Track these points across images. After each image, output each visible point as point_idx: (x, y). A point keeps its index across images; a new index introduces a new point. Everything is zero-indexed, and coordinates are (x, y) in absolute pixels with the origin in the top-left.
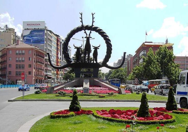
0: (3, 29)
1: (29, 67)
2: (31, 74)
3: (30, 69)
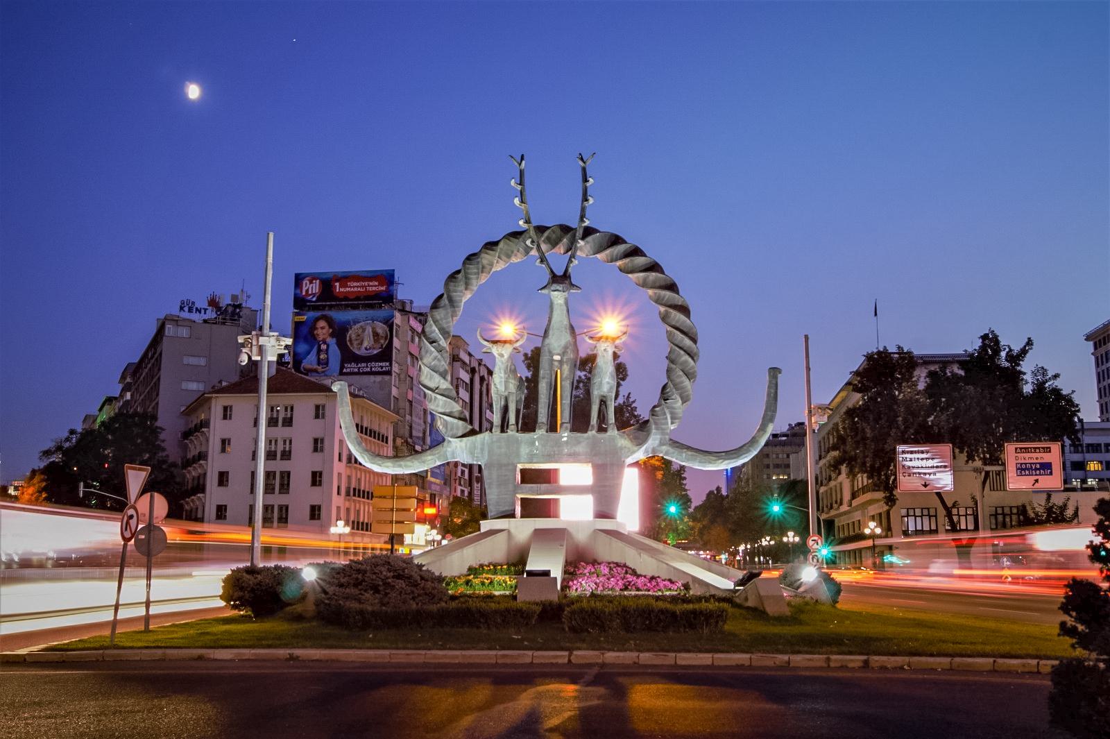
0: (205, 310)
1: (1050, 452)
2: (320, 485)
3: (315, 496)
